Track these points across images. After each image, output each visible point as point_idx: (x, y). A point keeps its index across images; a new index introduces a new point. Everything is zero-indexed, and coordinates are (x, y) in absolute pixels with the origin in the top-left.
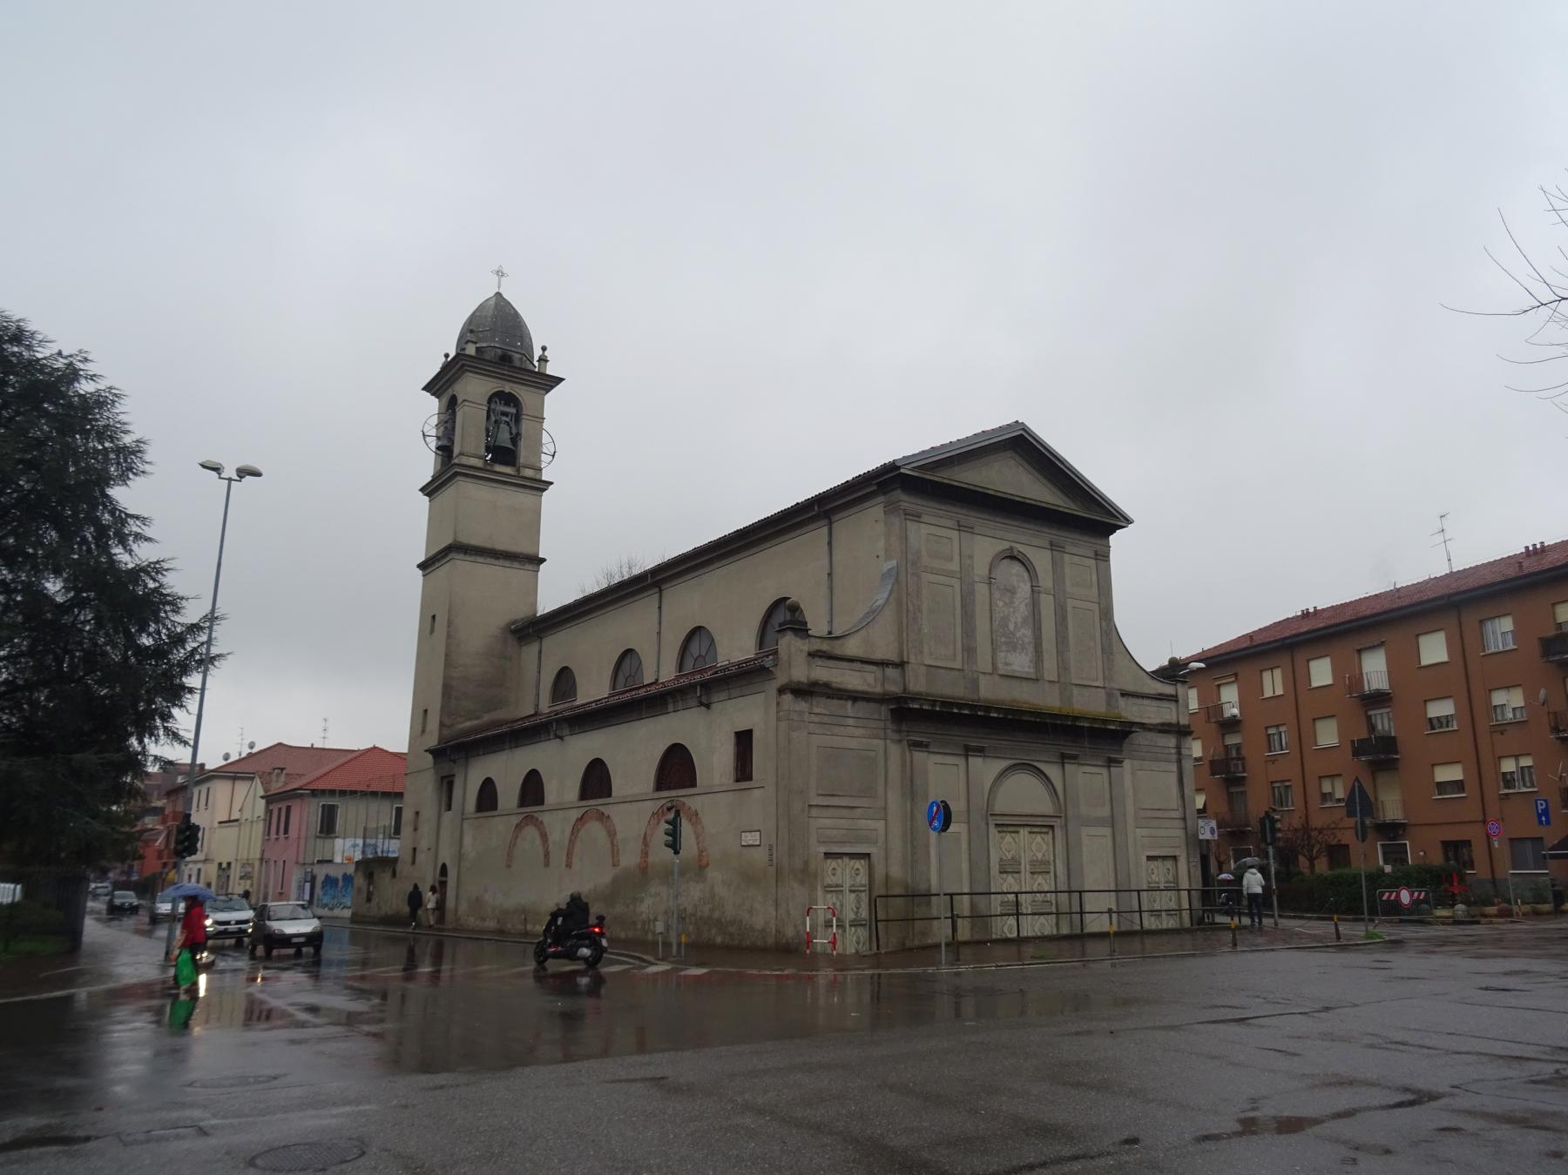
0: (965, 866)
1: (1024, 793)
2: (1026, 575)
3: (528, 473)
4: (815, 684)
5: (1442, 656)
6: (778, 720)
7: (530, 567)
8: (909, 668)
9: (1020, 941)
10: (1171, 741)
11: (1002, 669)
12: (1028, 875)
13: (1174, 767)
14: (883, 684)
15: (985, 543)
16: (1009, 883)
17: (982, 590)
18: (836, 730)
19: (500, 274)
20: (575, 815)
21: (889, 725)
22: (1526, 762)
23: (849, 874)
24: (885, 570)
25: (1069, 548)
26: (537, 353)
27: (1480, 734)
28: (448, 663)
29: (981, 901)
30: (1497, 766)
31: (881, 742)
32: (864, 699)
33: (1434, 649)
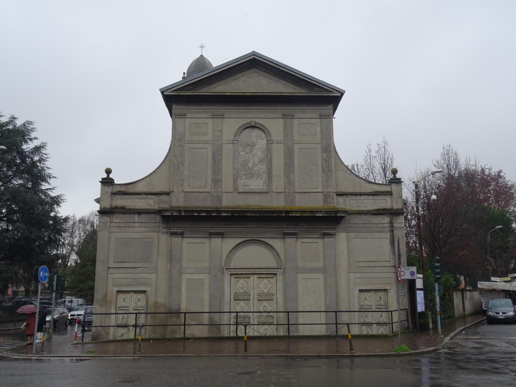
0: (206, 296)
1: (254, 255)
2: (263, 135)
4: (116, 208)
9: (185, 339)
10: (385, 220)
11: (241, 189)
12: (256, 302)
13: (388, 235)
14: (158, 204)
15: (232, 121)
16: (241, 306)
17: (227, 149)
18: (127, 230)
19: (202, 47)
21: (161, 225)
25: (297, 115)
29: (216, 317)
31: (156, 234)
32: (144, 213)
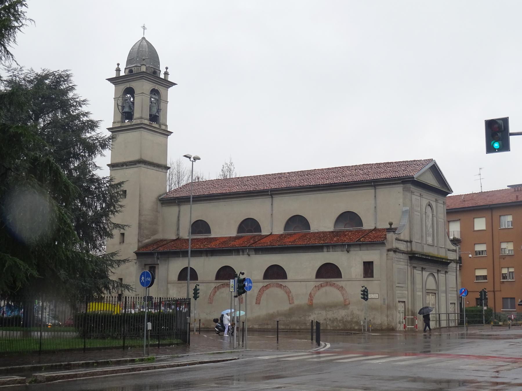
3: (163, 127)
5: (484, 228)
6: (387, 259)
7: (164, 171)
8: (413, 243)
13: (455, 274)
20: (213, 285)
22: (511, 270)
23: (401, 307)
24: (404, 210)
26: (163, 70)
27: (495, 258)
28: (140, 215)
30: (500, 271)
33: (480, 224)
